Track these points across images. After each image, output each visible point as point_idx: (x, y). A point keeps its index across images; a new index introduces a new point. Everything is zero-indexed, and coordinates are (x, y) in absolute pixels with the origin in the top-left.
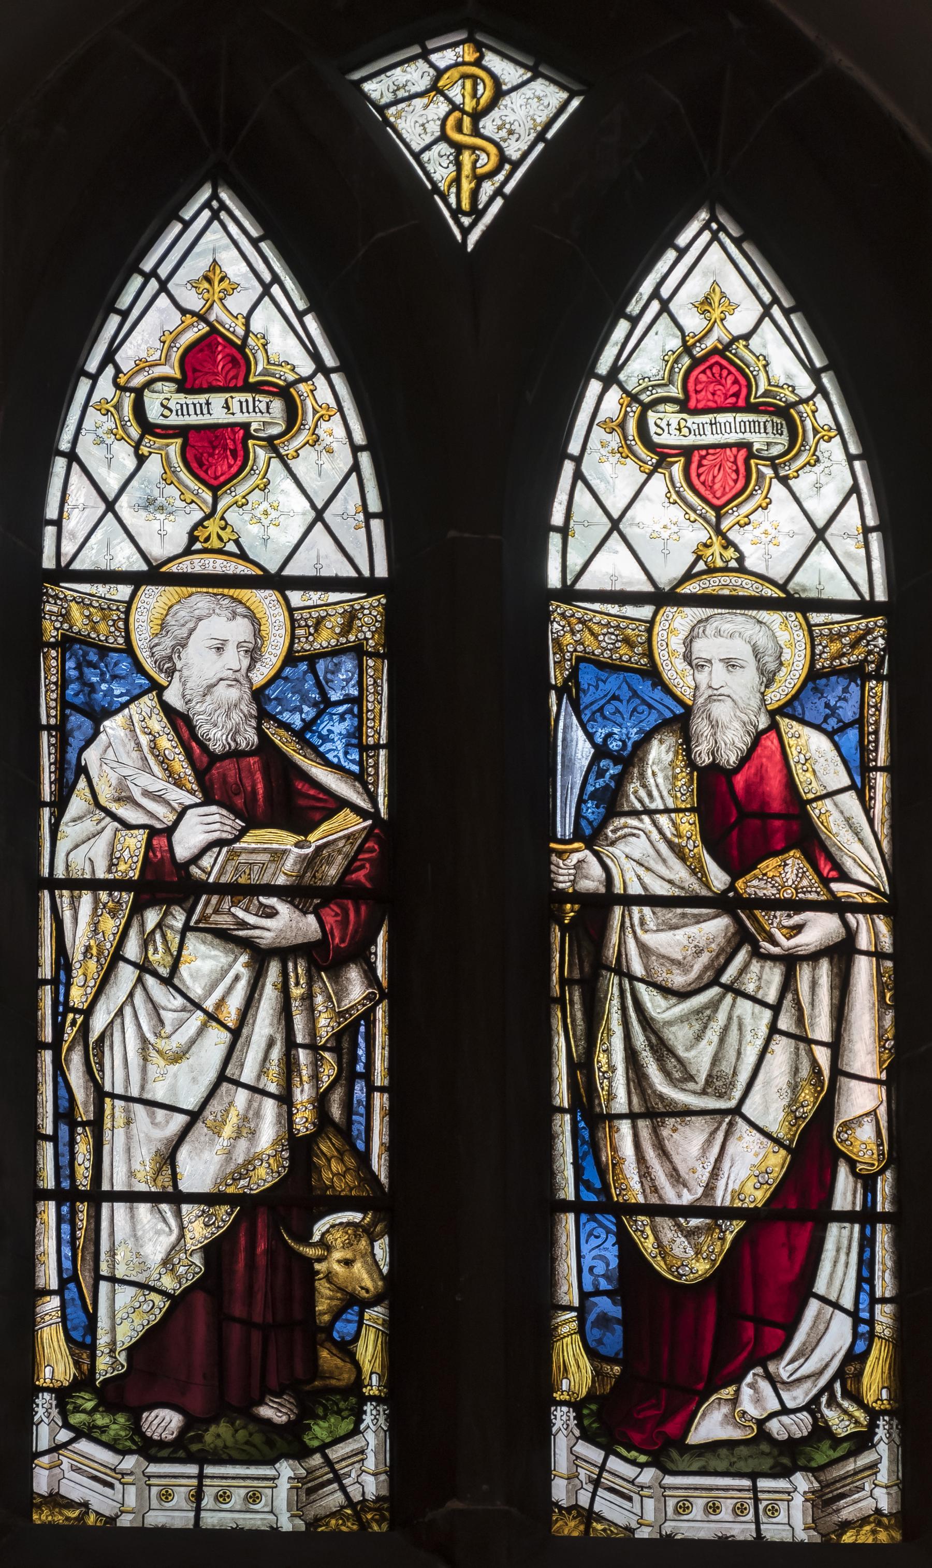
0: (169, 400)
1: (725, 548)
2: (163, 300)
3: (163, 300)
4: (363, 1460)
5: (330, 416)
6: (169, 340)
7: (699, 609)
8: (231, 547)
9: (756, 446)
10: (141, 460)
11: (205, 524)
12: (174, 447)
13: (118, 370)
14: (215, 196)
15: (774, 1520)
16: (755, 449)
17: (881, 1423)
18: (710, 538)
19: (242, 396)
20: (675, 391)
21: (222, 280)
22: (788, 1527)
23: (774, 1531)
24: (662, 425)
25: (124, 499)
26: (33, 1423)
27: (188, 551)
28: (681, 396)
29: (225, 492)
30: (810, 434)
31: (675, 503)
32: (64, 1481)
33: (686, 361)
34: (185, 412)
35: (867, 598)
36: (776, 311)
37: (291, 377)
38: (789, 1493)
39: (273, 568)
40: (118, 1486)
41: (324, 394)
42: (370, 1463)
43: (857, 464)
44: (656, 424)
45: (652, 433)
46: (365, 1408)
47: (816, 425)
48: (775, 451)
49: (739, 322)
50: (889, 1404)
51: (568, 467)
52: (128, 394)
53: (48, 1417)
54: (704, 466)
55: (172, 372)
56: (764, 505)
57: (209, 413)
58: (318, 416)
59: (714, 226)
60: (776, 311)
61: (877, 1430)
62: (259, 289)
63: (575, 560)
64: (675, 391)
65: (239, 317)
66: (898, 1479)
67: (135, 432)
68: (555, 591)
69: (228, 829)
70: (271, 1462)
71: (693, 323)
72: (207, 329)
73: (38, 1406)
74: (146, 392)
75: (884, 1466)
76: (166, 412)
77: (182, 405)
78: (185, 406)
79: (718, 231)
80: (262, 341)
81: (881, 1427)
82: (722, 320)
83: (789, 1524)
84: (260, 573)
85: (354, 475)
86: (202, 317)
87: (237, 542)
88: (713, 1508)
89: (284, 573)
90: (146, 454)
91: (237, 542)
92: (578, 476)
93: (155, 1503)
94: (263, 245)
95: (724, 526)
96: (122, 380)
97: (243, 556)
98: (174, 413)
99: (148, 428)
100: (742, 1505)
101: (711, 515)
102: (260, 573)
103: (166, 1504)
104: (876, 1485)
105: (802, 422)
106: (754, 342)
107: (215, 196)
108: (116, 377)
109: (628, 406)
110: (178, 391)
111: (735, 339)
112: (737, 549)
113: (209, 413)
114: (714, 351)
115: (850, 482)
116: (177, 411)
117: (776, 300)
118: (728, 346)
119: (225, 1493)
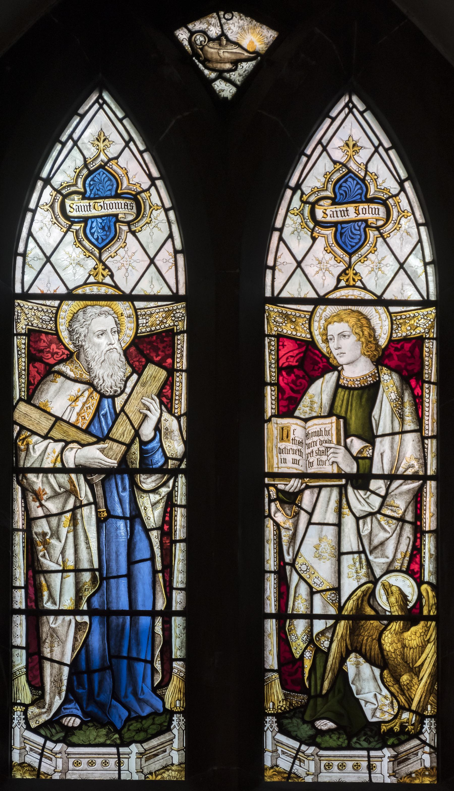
0: (326, 210)
1: (104, 270)
2: (75, 151)
3: (75, 151)
4: (172, 744)
5: (408, 216)
6: (328, 176)
7: (333, 307)
8: (359, 284)
9: (370, 221)
10: (314, 239)
11: (347, 272)
12: (330, 232)
13: (303, 193)
14: (350, 101)
15: (78, 768)
16: (119, 217)
17: (175, 718)
18: (97, 264)
19: (366, 206)
20: (329, 193)
21: (104, 140)
22: (381, 775)
23: (377, 778)
24: (73, 207)
25: (157, 258)
26: (12, 727)
27: (336, 288)
28: (82, 190)
29: (105, 250)
30: (148, 207)
31: (79, 247)
32: (27, 756)
33: (85, 172)
34: (80, 210)
35: (426, 298)
36: (381, 149)
37: (139, 190)
38: (128, 754)
39: (127, 291)
40: (54, 758)
41: (404, 204)
42: (176, 745)
43: (422, 229)
44: (70, 206)
45: (68, 211)
46: (425, 721)
47: (151, 204)
48: (130, 218)
49: (113, 151)
50: (180, 709)
51: (276, 235)
52: (308, 205)
53: (271, 728)
54: (93, 228)
55: (330, 194)
56: (123, 246)
57: (348, 215)
58: (152, 209)
59: (101, 101)
60: (381, 149)
61: (173, 722)
62: (124, 144)
63: (28, 279)
64: (329, 193)
65: (362, 164)
66: (183, 746)
67: (311, 225)
68: (18, 294)
69: (47, 425)
70: (381, 749)
71: (90, 152)
72: (347, 171)
73: (266, 722)
74: (316, 206)
75: (176, 741)
76: (325, 216)
77: (78, 207)
78: (80, 207)
79: (353, 107)
80: (126, 171)
81: (175, 721)
82: (104, 150)
83: (381, 774)
84: (121, 293)
85: (281, 242)
86: (344, 165)
87: (361, 281)
88: (91, 764)
89: (133, 293)
90: (317, 237)
91: (361, 281)
92: (281, 239)
93: (71, 766)
94: (125, 121)
95: (104, 257)
96: (305, 198)
97: (365, 288)
98: (329, 216)
99: (317, 223)
100: (106, 761)
101: (97, 252)
102: (121, 293)
103: (105, 768)
104: (424, 753)
105: (144, 202)
106: (121, 161)
107: (101, 97)
108: (301, 197)
109: (56, 196)
110: (332, 204)
111: (110, 160)
112: (110, 270)
113: (348, 215)
114: (101, 167)
115: (168, 233)
116: (331, 215)
117: (381, 144)
118: (106, 164)
119: (77, 761)
